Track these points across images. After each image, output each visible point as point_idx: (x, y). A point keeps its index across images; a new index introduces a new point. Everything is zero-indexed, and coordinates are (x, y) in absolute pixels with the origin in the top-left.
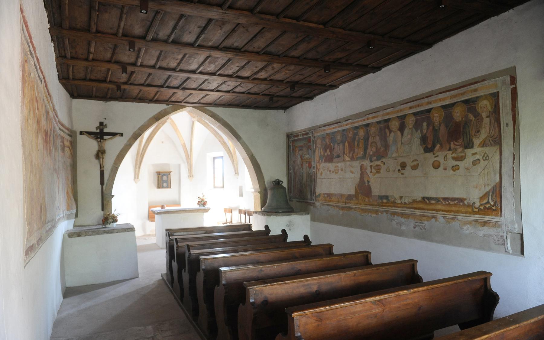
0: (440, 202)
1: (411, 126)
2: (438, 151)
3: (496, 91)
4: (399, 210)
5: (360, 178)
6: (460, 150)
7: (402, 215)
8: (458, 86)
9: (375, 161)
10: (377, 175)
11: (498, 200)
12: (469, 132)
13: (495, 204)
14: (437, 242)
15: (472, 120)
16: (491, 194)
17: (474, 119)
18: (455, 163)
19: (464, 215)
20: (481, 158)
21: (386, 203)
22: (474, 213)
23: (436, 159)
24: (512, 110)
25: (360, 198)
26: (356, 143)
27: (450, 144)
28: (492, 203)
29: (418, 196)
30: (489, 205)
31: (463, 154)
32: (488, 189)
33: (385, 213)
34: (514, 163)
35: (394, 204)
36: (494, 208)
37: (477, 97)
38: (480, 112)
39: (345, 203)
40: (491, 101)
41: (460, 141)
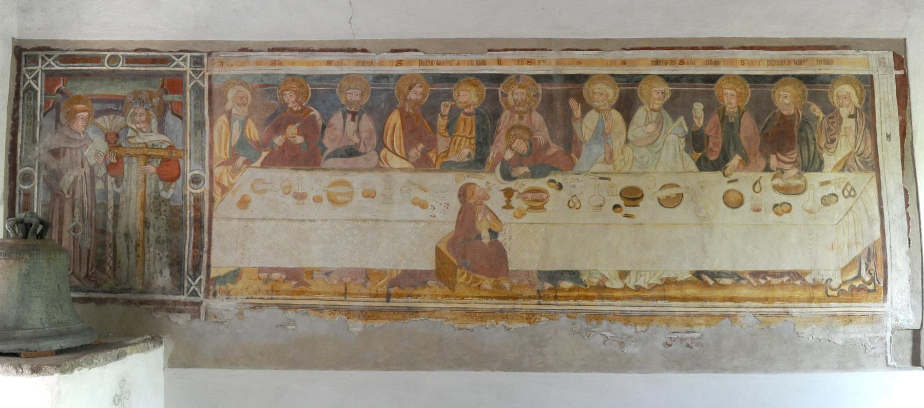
0: (743, 282)
1: (657, 105)
2: (737, 169)
3: (867, 73)
4: (618, 306)
5: (460, 223)
6: (794, 171)
7: (626, 318)
8: (786, 45)
9: (525, 176)
10: (531, 217)
11: (880, 271)
12: (814, 139)
13: (872, 280)
14: (735, 370)
15: (818, 118)
16: (863, 261)
17: (822, 115)
18: (781, 198)
19: (806, 305)
20: (839, 192)
21: (571, 290)
22: (828, 298)
23: (731, 186)
24: (900, 114)
25: (460, 280)
26: (442, 122)
27: (768, 158)
28: (867, 279)
29: (684, 271)
30: (861, 282)
31: (799, 182)
32: (857, 251)
33: (564, 319)
34: (907, 206)
35: (601, 291)
36: (871, 287)
37: (832, 76)
38: (837, 105)
39: (388, 296)
40: (858, 89)
41: (794, 155)
